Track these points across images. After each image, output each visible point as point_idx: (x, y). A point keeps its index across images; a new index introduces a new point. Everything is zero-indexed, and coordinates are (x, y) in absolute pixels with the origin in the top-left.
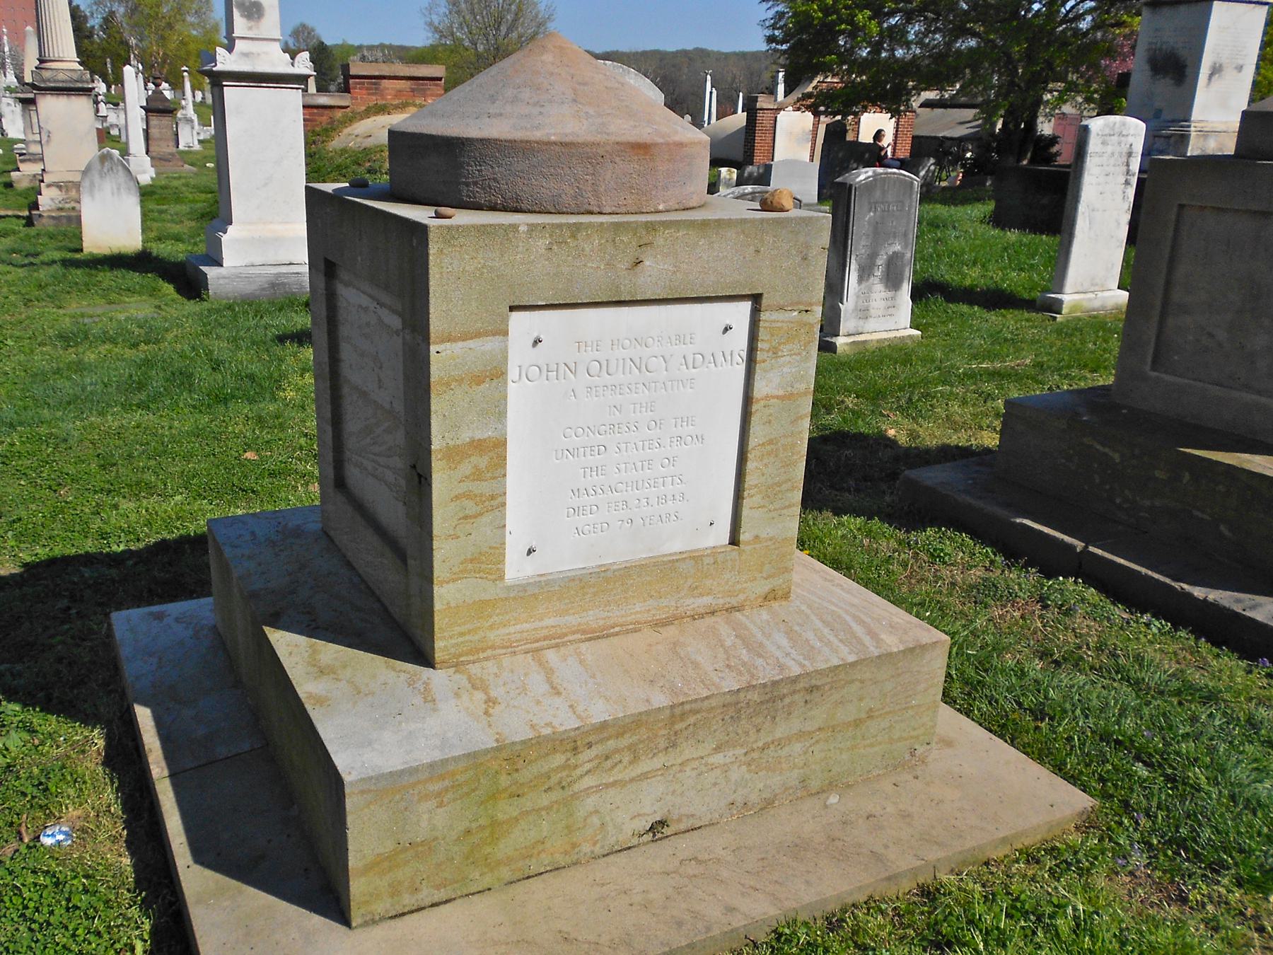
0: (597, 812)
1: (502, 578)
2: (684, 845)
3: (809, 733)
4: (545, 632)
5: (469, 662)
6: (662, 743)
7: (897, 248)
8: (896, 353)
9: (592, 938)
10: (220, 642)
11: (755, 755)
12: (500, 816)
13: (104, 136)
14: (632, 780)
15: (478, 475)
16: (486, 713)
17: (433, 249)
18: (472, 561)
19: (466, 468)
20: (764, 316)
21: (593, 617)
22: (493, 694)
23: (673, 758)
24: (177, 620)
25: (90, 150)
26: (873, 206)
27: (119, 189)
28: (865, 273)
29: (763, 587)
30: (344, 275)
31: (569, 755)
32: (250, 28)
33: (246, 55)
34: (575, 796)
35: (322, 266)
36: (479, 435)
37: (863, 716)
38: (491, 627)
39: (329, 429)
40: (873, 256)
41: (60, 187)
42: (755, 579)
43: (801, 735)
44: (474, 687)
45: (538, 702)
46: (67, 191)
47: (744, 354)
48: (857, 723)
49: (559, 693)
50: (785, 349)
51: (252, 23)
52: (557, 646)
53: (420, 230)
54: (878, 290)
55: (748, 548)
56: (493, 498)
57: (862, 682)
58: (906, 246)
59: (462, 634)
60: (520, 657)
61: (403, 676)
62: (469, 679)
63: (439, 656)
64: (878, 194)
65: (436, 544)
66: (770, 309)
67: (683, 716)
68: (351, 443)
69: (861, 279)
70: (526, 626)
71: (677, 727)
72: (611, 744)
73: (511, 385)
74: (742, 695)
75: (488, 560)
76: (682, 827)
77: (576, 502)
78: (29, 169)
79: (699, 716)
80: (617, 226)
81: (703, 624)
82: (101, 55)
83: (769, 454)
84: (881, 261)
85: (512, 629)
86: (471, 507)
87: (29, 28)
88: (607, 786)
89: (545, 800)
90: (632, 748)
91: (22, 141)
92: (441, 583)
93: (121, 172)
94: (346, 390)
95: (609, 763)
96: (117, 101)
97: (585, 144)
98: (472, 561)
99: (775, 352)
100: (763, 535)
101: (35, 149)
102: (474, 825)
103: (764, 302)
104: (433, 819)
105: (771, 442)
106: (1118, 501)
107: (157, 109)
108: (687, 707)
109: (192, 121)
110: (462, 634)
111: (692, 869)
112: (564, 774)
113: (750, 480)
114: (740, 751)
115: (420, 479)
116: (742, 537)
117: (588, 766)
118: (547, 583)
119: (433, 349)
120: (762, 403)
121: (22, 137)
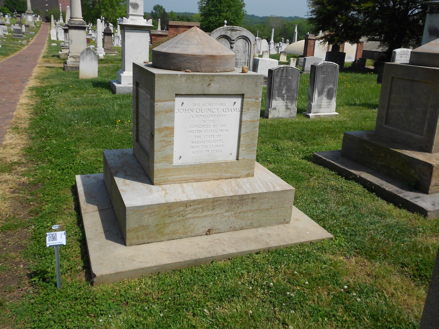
0: (192, 224)
1: (172, 163)
2: (216, 236)
3: (253, 210)
4: (183, 179)
5: (163, 184)
6: (211, 208)
7: (331, 86)
8: (329, 120)
9: (187, 253)
10: (104, 183)
11: (237, 215)
12: (166, 222)
13: (89, 41)
14: (202, 217)
15: (166, 136)
16: (165, 196)
17: (156, 79)
18: (164, 158)
19: (163, 134)
20: (245, 100)
21: (197, 176)
22: (167, 192)
23: (214, 212)
24: (93, 178)
25: (84, 46)
26: (323, 73)
27: (92, 59)
28: (320, 94)
29: (247, 172)
30: (140, 86)
31: (185, 207)
32: (134, 12)
33: (132, 20)
34: (187, 219)
35: (135, 83)
36: (167, 126)
37: (269, 208)
38: (169, 176)
39: (135, 126)
40: (323, 89)
41: (74, 58)
42: (243, 170)
43: (251, 211)
44: (163, 190)
45: (178, 194)
46: (76, 59)
47: (240, 109)
48: (267, 210)
49: (184, 193)
50: (251, 109)
51: (135, 10)
52: (187, 182)
53: (153, 75)
54: (325, 100)
55: (241, 161)
56: (170, 142)
57: (269, 198)
58: (334, 86)
59: (161, 177)
60: (177, 184)
61: (145, 187)
62: (162, 188)
63: (155, 182)
64: (325, 70)
65: (155, 153)
66: (247, 98)
67: (216, 201)
68: (140, 129)
69: (319, 95)
70: (179, 176)
71: (215, 204)
72: (196, 206)
73: (176, 114)
74: (233, 197)
75: (169, 158)
76: (216, 232)
77: (193, 145)
78: (65, 51)
79: (221, 202)
80: (204, 75)
81: (227, 181)
82: (90, 16)
83: (247, 136)
84: (326, 90)
85: (175, 177)
86: (164, 144)
87: (68, 7)
88: (195, 217)
89: (178, 219)
90: (202, 208)
91: (64, 42)
92: (156, 163)
93: (93, 54)
94: (140, 115)
95: (196, 211)
96: (95, 30)
97: (197, 55)
98: (164, 158)
99: (248, 109)
100: (245, 158)
101: (67, 45)
102: (159, 223)
103: (245, 96)
104: (149, 220)
105: (247, 133)
106: (372, 163)
107: (107, 33)
108: (218, 199)
109: (119, 37)
110: (161, 177)
111: (217, 241)
112: (183, 213)
113: (241, 143)
114: (233, 213)
115: (152, 136)
116: (239, 158)
117: (190, 211)
118: (185, 165)
119: (156, 103)
120: (245, 122)
121: (64, 40)
